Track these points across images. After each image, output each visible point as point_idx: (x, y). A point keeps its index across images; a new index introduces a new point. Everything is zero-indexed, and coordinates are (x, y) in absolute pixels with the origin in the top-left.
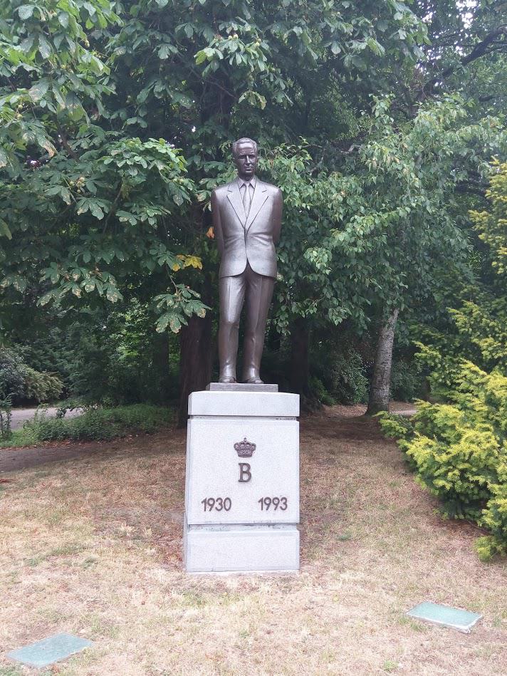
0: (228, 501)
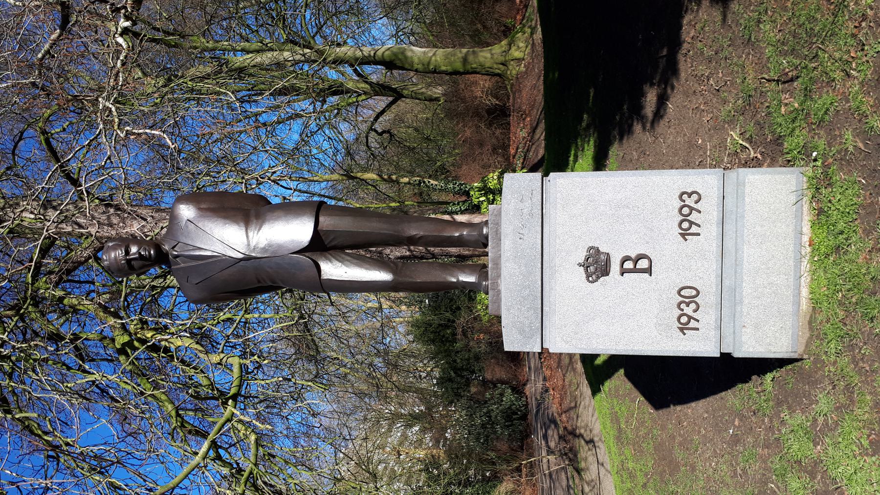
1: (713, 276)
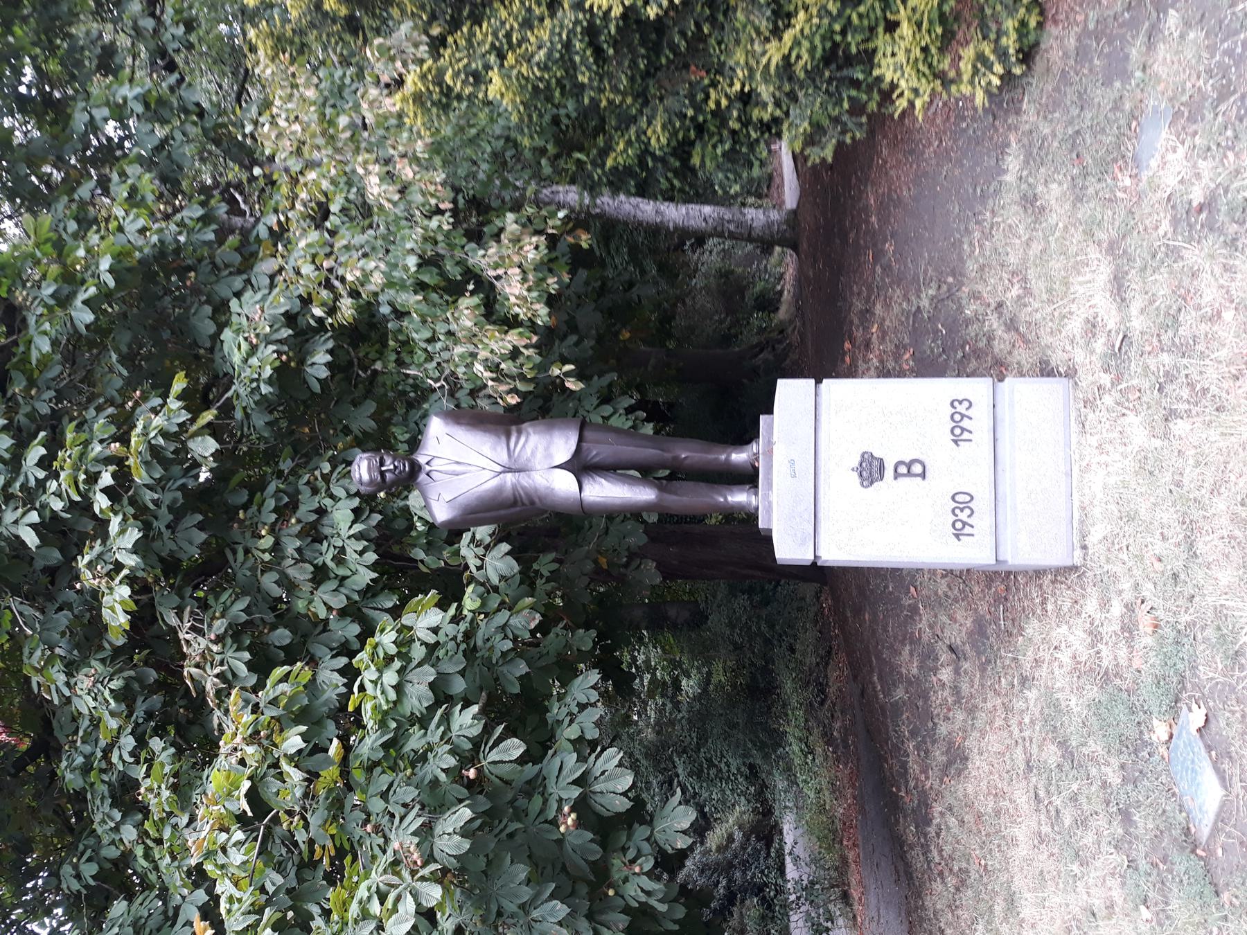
0: (958, 498)
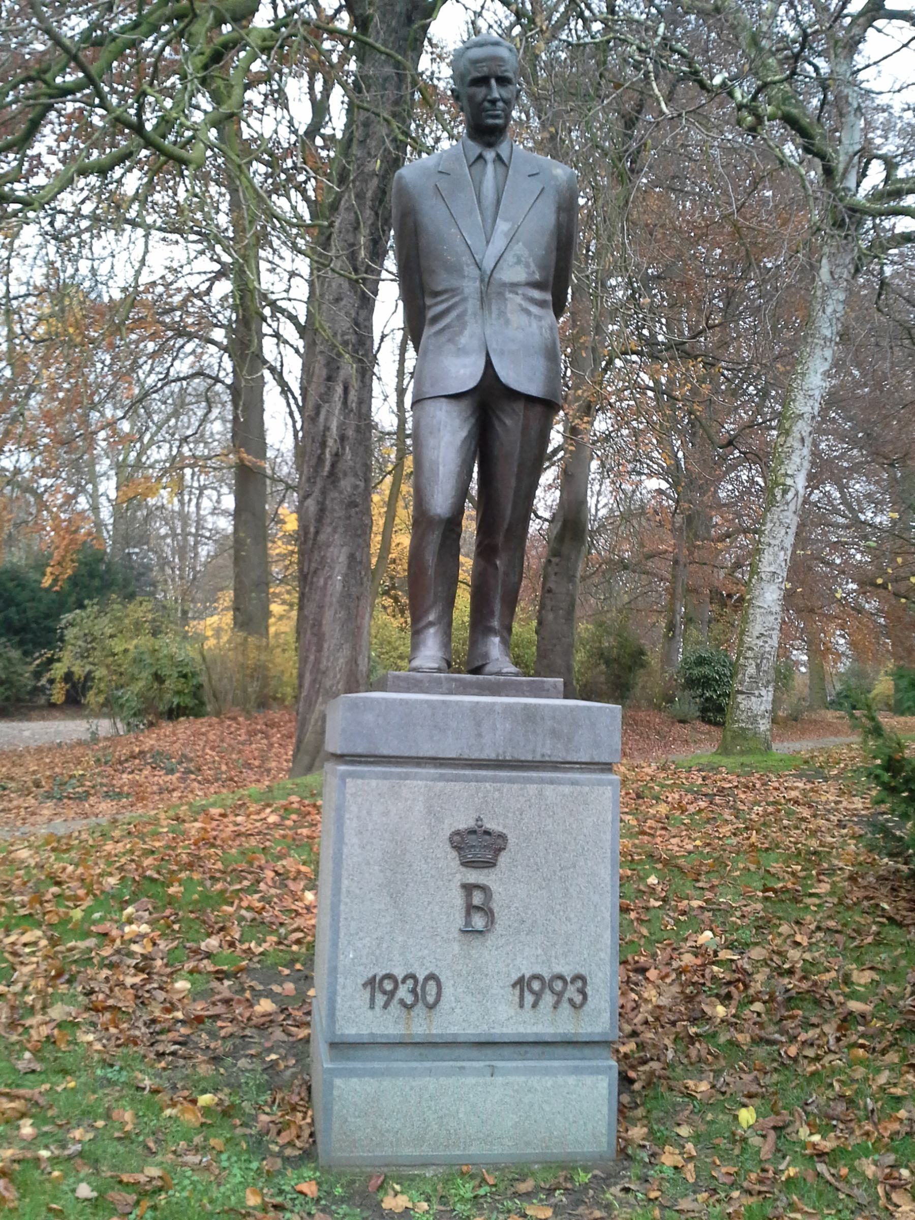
0: (432, 985)
1: (453, 1030)
